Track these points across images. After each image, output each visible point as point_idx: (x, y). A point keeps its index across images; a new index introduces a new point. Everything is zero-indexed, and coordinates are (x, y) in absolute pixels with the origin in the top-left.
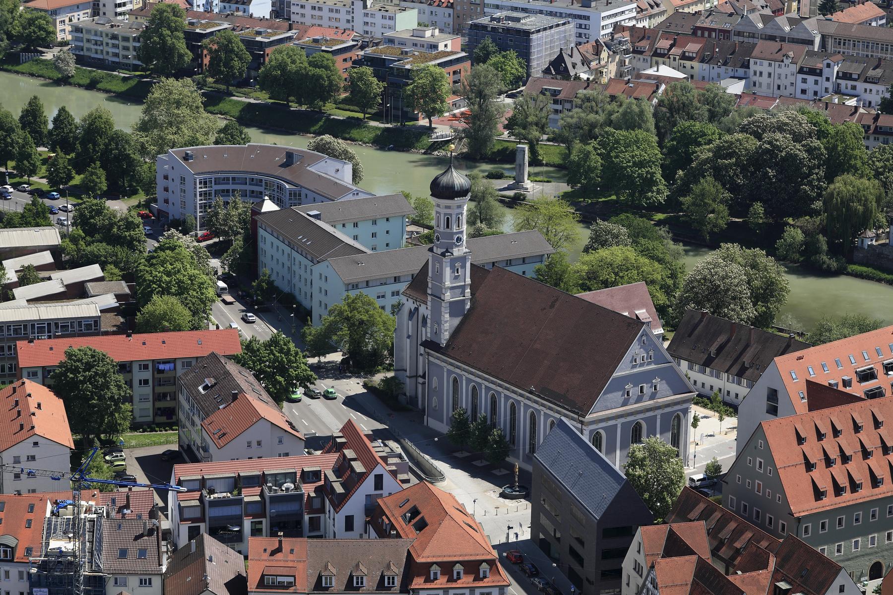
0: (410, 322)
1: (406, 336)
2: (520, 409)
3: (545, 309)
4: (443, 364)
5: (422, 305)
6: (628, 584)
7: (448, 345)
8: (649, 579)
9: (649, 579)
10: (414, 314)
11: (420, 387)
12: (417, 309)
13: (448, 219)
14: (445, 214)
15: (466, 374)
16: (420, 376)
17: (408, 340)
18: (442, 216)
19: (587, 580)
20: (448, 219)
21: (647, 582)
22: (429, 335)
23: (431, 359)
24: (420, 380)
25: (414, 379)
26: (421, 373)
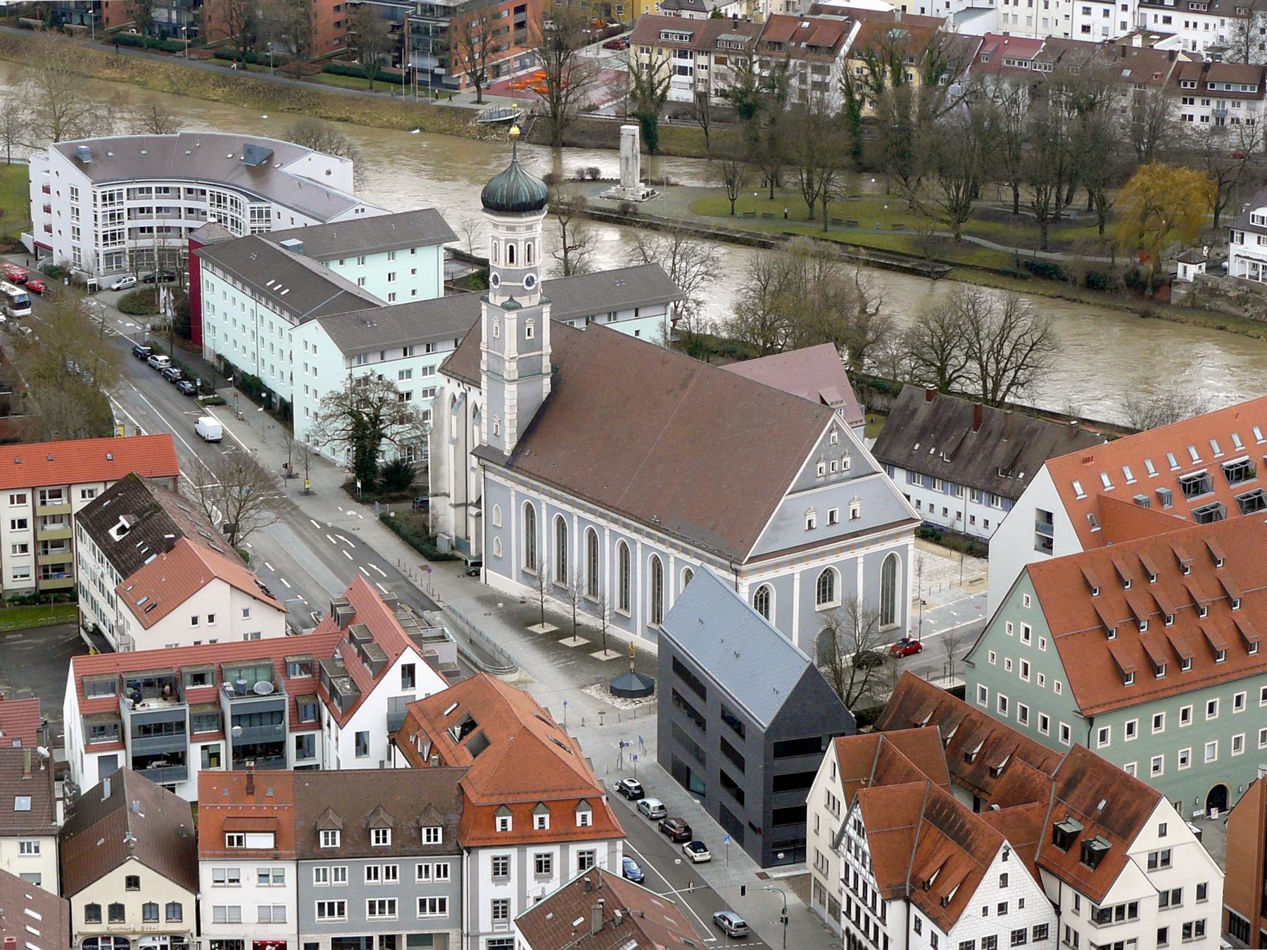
3: (672, 390)
4: (509, 484)
5: (472, 388)
6: (817, 832)
7: (516, 452)
8: (851, 821)
9: (851, 821)
10: (460, 403)
11: (472, 522)
12: (465, 396)
13: (511, 248)
14: (507, 241)
15: (547, 499)
16: (472, 504)
18: (502, 243)
19: (751, 825)
20: (511, 248)
21: (848, 826)
22: (485, 437)
23: (490, 475)
24: (473, 511)
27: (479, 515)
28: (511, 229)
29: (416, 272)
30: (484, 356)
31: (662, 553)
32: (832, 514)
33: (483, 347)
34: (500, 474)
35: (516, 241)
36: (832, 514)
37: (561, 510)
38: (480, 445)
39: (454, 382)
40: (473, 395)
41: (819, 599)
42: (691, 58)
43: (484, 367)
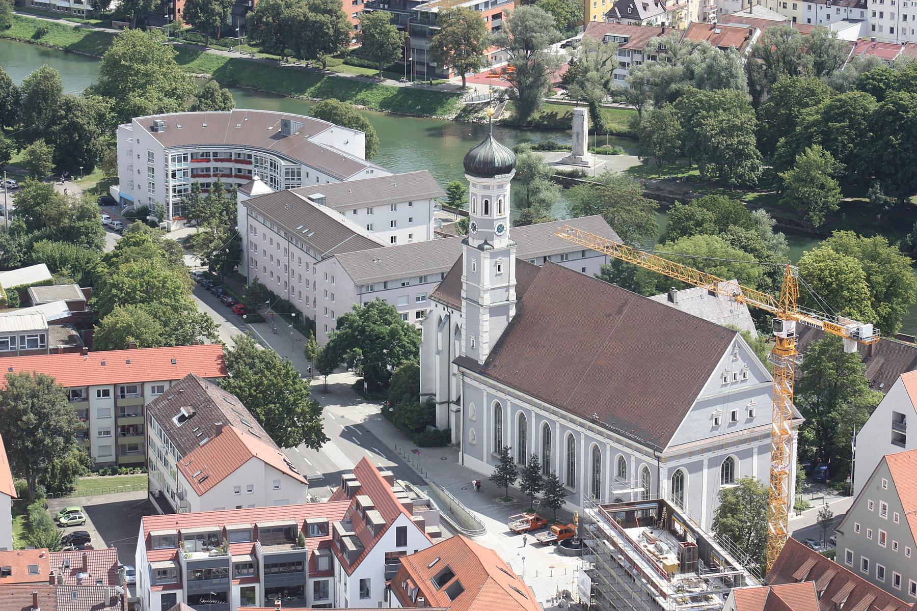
0: (440, 334)
1: (434, 350)
2: (580, 443)
3: (610, 315)
4: (482, 387)
7: (488, 362)
12: (448, 317)
13: (486, 202)
14: (483, 197)
15: (511, 399)
16: (453, 402)
17: (438, 357)
18: (479, 199)
22: (464, 350)
23: (467, 380)
24: (454, 407)
25: (446, 406)
26: (454, 398)
27: (458, 411)
28: (486, 187)
29: (254, 490)
30: (464, 286)
31: (601, 443)
32: (734, 413)
33: (463, 279)
34: (475, 379)
35: (490, 197)
36: (734, 413)
37: (521, 408)
38: (460, 356)
39: (440, 307)
40: (456, 318)
41: (722, 480)
42: (629, 56)
43: (463, 294)
